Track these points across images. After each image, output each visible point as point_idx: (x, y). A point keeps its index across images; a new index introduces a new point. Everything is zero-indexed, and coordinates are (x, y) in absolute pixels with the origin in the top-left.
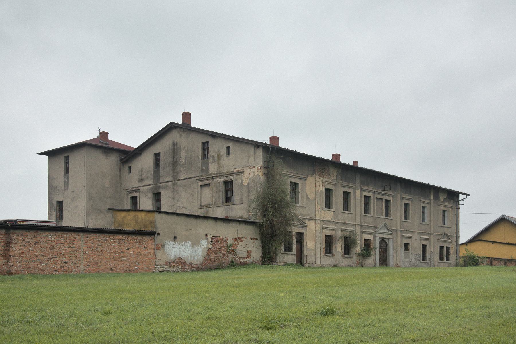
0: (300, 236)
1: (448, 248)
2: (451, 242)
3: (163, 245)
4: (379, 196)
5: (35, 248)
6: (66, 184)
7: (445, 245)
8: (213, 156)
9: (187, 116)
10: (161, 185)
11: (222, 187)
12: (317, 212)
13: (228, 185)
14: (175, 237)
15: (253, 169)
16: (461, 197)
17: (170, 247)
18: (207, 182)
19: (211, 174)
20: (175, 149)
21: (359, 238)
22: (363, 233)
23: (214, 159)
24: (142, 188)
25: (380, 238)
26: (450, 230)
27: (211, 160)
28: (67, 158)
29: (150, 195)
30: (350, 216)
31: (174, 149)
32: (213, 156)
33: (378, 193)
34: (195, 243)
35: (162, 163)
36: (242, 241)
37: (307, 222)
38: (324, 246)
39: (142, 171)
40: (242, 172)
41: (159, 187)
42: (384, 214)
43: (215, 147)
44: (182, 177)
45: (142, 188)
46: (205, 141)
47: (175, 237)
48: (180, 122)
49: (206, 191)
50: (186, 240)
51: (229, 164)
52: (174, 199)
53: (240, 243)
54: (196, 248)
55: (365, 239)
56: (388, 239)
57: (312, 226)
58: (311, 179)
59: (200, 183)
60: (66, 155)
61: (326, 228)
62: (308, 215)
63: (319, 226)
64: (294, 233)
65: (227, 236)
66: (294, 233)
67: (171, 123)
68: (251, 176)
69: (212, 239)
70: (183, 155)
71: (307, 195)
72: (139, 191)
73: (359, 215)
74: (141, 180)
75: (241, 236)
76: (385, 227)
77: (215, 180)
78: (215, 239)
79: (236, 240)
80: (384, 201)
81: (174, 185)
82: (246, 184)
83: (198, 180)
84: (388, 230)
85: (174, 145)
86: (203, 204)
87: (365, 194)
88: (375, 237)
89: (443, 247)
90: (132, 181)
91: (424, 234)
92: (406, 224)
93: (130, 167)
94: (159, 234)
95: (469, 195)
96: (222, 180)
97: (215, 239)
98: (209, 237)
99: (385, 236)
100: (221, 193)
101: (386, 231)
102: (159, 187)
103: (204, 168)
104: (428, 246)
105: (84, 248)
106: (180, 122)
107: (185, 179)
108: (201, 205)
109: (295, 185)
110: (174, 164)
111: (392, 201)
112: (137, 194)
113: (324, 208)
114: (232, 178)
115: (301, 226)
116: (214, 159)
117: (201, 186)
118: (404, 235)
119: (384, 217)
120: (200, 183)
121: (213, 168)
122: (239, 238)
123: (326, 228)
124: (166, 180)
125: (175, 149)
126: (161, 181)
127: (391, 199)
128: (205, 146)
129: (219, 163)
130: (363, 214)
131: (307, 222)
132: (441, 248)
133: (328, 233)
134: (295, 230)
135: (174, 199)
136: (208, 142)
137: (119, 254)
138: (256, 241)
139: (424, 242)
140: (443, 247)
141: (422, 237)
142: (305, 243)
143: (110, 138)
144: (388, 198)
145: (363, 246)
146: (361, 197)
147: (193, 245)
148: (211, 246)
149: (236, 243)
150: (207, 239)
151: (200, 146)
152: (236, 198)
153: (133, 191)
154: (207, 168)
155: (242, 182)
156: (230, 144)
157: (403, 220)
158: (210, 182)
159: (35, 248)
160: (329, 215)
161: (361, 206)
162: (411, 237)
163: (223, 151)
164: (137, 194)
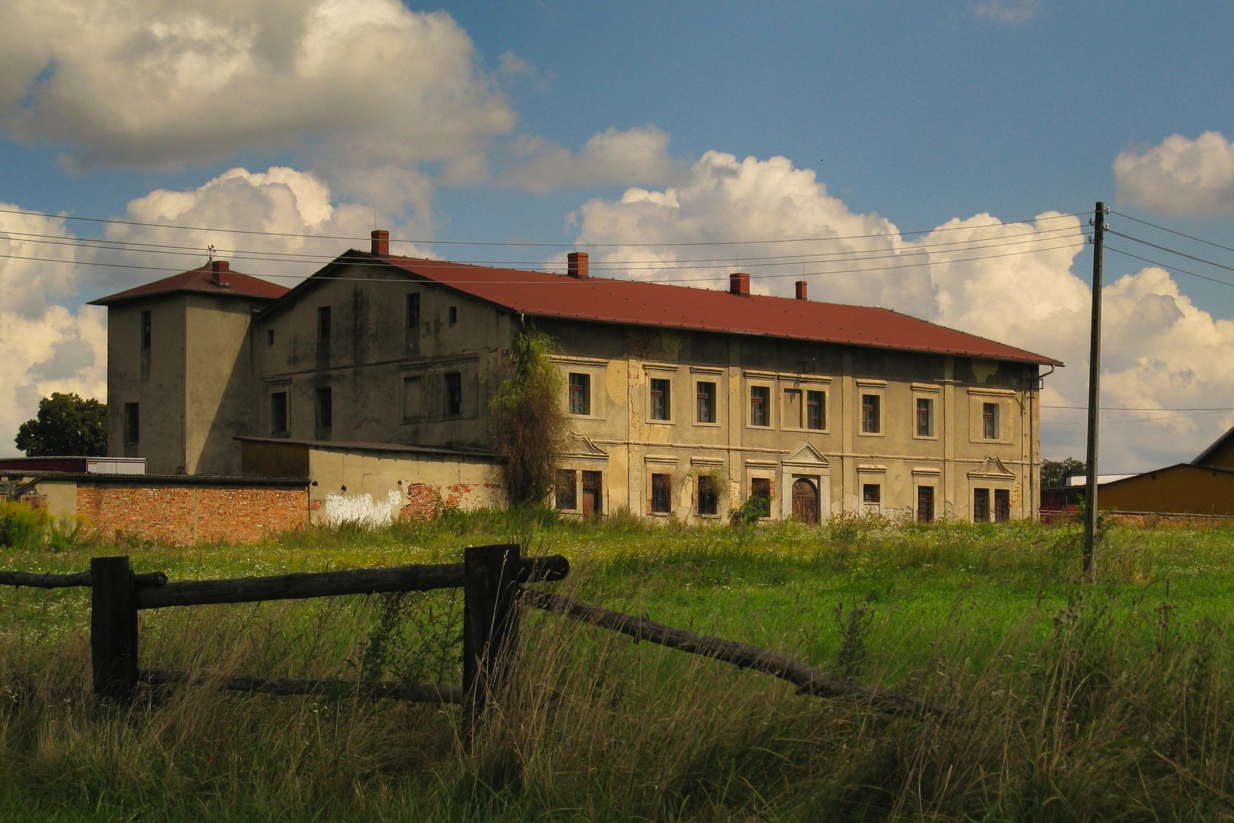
0: (594, 481)
1: (1002, 495)
2: (1012, 478)
3: (323, 502)
4: (791, 385)
5: (132, 510)
6: (146, 369)
7: (992, 486)
8: (428, 324)
9: (379, 238)
10: (332, 372)
11: (443, 385)
12: (631, 429)
13: (453, 380)
14: (344, 488)
15: (494, 354)
16: (1043, 369)
17: (336, 504)
18: (417, 373)
19: (425, 358)
20: (358, 302)
21: (737, 475)
22: (747, 465)
23: (428, 329)
24: (295, 377)
25: (794, 475)
26: (1008, 450)
27: (423, 330)
28: (147, 322)
29: (312, 392)
30: (714, 431)
31: (356, 302)
32: (428, 324)
33: (787, 379)
34: (380, 497)
35: (333, 328)
36: (468, 491)
37: (609, 449)
38: (650, 496)
39: (295, 342)
40: (475, 358)
41: (329, 377)
42: (805, 423)
43: (433, 307)
44: (372, 360)
45: (295, 377)
46: (412, 292)
47: (344, 488)
48: (367, 248)
49: (415, 390)
50: (363, 493)
51: (457, 339)
52: (355, 402)
53: (466, 495)
54: (380, 505)
55: (754, 480)
56: (818, 477)
57: (619, 455)
58: (616, 365)
59: (403, 375)
60: (146, 309)
61: (655, 461)
62: (611, 436)
63: (637, 455)
64: (579, 473)
65: (439, 484)
66: (579, 473)
67: (351, 253)
68: (492, 366)
69: (410, 488)
70: (373, 315)
71: (608, 397)
72: (289, 382)
73: (738, 430)
74: (294, 361)
75: (466, 483)
76: (808, 452)
77: (431, 370)
78: (415, 490)
79: (456, 489)
80: (805, 395)
81: (356, 373)
82: (482, 382)
83: (400, 369)
84: (817, 457)
85: (357, 294)
86: (409, 415)
87: (752, 382)
88: (780, 475)
89: (987, 491)
90: (276, 361)
91: (924, 462)
92: (869, 443)
93: (271, 333)
94: (315, 484)
95: (1061, 365)
96: (443, 370)
97: (415, 490)
98: (405, 486)
99: (807, 471)
100: (441, 396)
101: (813, 460)
102: (329, 377)
103: (411, 345)
104: (936, 490)
105: (199, 507)
106: (367, 248)
107: (376, 364)
108: (405, 418)
109: (581, 383)
110: (357, 332)
111: (827, 394)
112: (286, 389)
113: (649, 420)
114: (459, 367)
115: (593, 458)
116: (428, 329)
117: (407, 380)
118: (861, 466)
119: (805, 429)
120: (403, 375)
121: (426, 346)
122: (464, 486)
123: (655, 461)
124: (342, 364)
125: (358, 302)
126: (332, 364)
127: (825, 388)
128: (413, 302)
129: (437, 338)
130: (749, 425)
131: (609, 449)
132: (981, 494)
133: (657, 468)
134: (580, 466)
135: (355, 402)
136: (418, 295)
137: (252, 518)
138: (500, 491)
139: (925, 482)
140: (987, 491)
141: (916, 469)
142: (604, 492)
143: (231, 268)
144: (816, 387)
145: (750, 494)
146: (743, 390)
147: (375, 502)
148: (409, 502)
149: (457, 494)
150: (401, 490)
151: (404, 302)
152: (466, 406)
153: (277, 383)
154: (417, 348)
155: (477, 375)
156: (456, 303)
157: (861, 433)
158: (421, 373)
159: (132, 510)
160: (661, 432)
161: (744, 408)
162: (882, 471)
163: (445, 316)
164: (286, 389)
